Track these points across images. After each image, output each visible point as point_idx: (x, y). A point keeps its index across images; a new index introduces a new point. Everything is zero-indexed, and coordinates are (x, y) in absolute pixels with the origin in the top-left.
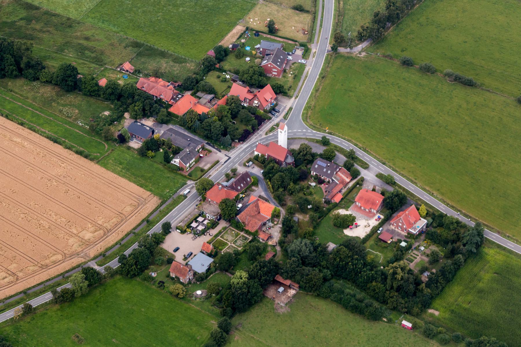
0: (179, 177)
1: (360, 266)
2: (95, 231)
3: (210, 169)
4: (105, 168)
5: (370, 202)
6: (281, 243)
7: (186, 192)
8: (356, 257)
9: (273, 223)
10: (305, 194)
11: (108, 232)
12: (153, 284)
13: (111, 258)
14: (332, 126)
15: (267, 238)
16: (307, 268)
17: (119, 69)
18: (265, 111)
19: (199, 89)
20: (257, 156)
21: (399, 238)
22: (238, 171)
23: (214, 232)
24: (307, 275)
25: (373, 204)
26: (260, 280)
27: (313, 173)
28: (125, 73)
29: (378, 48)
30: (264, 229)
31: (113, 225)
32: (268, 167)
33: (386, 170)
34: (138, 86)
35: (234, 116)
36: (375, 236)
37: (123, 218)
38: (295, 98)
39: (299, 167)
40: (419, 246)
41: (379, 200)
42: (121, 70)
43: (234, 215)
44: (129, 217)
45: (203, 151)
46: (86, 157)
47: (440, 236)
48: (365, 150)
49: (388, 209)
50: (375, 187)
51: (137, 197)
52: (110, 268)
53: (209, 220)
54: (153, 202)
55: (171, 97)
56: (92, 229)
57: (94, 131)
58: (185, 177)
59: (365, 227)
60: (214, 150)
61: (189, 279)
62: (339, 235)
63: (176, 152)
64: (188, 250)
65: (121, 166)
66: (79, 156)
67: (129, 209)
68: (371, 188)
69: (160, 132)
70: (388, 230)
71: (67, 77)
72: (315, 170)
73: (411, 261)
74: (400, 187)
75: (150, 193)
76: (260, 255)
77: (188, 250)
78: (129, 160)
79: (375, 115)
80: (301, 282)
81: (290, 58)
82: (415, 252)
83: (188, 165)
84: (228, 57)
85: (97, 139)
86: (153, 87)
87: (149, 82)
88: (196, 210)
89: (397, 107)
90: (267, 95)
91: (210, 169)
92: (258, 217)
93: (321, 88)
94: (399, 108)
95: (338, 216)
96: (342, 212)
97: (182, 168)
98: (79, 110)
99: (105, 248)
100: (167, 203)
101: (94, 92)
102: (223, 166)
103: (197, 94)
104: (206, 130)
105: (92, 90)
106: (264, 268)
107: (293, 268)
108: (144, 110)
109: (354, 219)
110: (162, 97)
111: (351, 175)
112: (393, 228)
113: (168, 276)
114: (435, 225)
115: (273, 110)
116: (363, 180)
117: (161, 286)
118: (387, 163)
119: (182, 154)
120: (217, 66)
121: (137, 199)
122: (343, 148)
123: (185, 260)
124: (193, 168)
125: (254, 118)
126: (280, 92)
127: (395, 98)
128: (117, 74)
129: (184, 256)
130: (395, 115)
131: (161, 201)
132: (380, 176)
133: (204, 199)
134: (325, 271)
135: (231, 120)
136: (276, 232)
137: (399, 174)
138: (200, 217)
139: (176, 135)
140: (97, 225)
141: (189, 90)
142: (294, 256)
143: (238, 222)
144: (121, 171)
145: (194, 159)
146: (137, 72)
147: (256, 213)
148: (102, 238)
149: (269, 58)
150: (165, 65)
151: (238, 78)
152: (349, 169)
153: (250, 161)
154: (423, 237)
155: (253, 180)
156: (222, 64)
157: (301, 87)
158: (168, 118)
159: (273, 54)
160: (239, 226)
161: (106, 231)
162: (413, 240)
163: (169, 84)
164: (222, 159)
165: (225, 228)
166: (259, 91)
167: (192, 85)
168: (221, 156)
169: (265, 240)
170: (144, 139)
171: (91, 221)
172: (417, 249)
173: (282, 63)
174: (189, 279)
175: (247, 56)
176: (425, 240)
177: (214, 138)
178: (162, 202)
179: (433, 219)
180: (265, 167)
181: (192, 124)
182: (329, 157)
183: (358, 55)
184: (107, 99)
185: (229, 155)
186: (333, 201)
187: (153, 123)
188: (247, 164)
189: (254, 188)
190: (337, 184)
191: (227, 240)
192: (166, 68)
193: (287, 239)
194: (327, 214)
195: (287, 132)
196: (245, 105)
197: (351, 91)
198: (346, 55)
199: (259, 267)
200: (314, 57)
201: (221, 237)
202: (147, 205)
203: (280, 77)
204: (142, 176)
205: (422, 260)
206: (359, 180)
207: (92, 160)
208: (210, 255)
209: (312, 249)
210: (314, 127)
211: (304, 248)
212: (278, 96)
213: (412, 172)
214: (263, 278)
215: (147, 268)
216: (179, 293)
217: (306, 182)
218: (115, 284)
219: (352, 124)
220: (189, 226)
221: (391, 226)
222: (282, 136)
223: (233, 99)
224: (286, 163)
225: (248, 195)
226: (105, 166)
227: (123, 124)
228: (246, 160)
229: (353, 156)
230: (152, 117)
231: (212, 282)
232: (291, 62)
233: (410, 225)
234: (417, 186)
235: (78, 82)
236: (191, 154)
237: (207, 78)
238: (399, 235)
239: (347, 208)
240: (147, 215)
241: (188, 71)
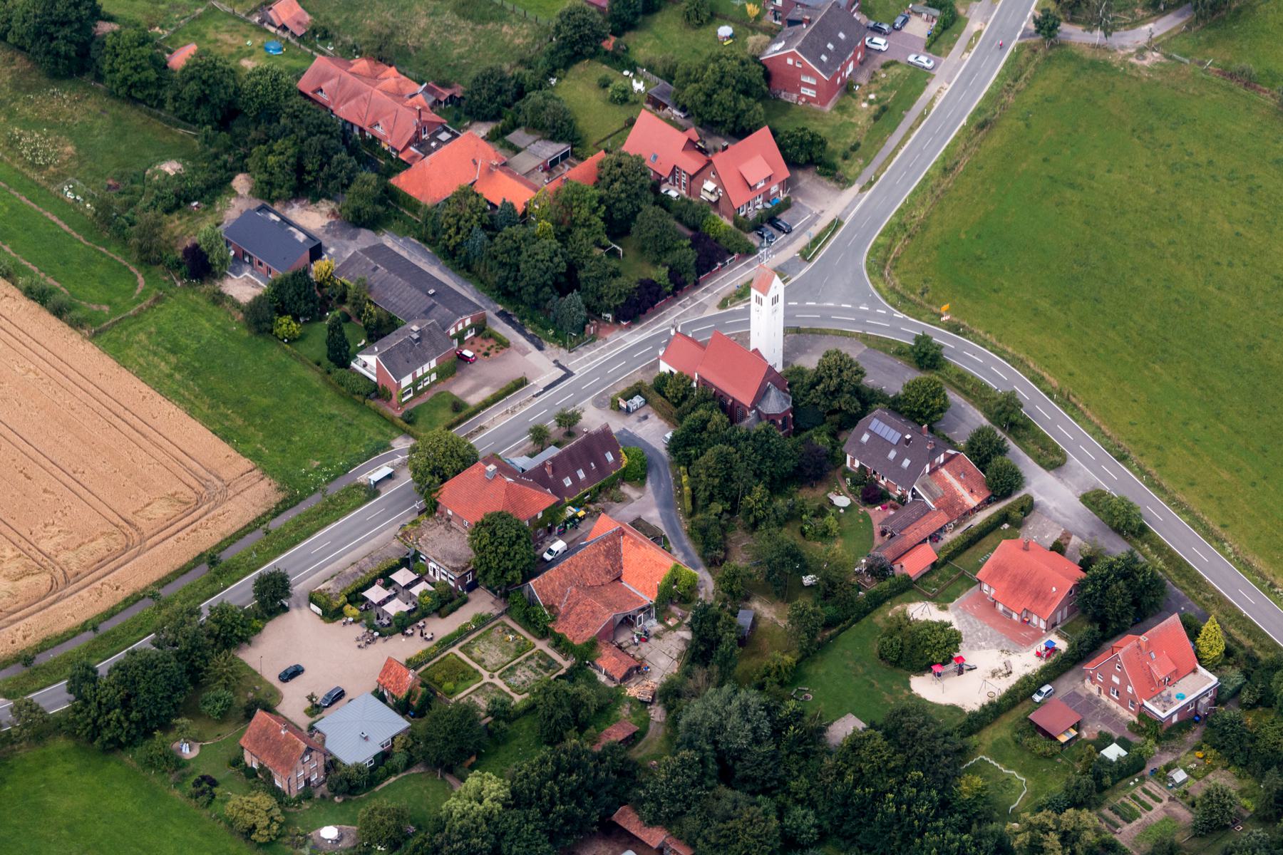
0: (367, 419)
1: (923, 810)
2: (24, 574)
3: (486, 404)
4: (117, 359)
5: (1025, 587)
6: (670, 694)
7: (376, 476)
8: (916, 774)
9: (661, 621)
10: (803, 534)
11: (67, 582)
12: (177, 785)
13: (50, 674)
14: (968, 303)
15: (623, 670)
16: (730, 793)
17: (257, 19)
18: (739, 224)
19: (521, 118)
20: (663, 380)
21: (1106, 729)
22: (582, 422)
23: (440, 628)
24: (726, 818)
25: (1040, 595)
26: (545, 813)
27: (853, 463)
28: (275, 35)
29: (1210, 42)
30: (625, 638)
31: (90, 560)
32: (686, 422)
33: (1120, 481)
34: (305, 84)
35: (618, 227)
36: (1019, 711)
37: (132, 540)
38: (862, 190)
39: (804, 435)
40: (1168, 768)
41: (1062, 579)
42: (262, 22)
43: (518, 573)
44: (156, 539)
45: (478, 341)
46: (59, 312)
47: (1253, 740)
48: (1065, 402)
49: (1091, 622)
50: (1067, 535)
51: (202, 472)
52: (33, 708)
53: (433, 584)
54: (253, 495)
55: (411, 134)
56: (14, 566)
57: (108, 223)
58: (390, 422)
59: (994, 674)
60: (522, 340)
61: (308, 782)
62: (891, 692)
63: (378, 330)
64: (332, 680)
65: (173, 359)
66: (35, 306)
67: (160, 511)
68: (1051, 536)
69: (345, 255)
70: (1073, 697)
71: (54, 23)
72: (861, 450)
73: (1129, 817)
74: (1160, 548)
75: (250, 466)
76: (582, 728)
77: (332, 680)
78: (209, 342)
79: (1138, 282)
80: (699, 841)
81: (880, 42)
82: (1152, 786)
83: (407, 381)
84: (659, 18)
85: (113, 253)
86: (355, 94)
87: (345, 75)
88: (395, 544)
89: (1224, 261)
90: (755, 164)
91: (486, 404)
92: (609, 593)
93: (965, 161)
94: (1230, 265)
95: (903, 623)
96: (922, 612)
97: (385, 389)
98: (79, 147)
99: (43, 635)
100: (303, 507)
101: (146, 87)
102: (537, 401)
103: (510, 138)
104: (502, 265)
105: (136, 78)
106: (570, 773)
107: (677, 787)
108: (299, 169)
109: (954, 640)
110: (380, 131)
111: (989, 485)
112: (1094, 689)
113: (237, 762)
114: (1245, 697)
115: (771, 221)
116: (1028, 507)
117: (203, 792)
118: (1133, 455)
119: (393, 340)
120: (609, 44)
121: (198, 478)
122: (987, 386)
123: (312, 715)
124: (427, 396)
125: (688, 242)
126: (810, 163)
127: (1227, 226)
128: (246, 37)
129: (310, 698)
130: (1211, 288)
131: (282, 495)
132: (1093, 500)
133: (432, 508)
134: (799, 811)
135: (605, 240)
136: (664, 655)
137: (1168, 503)
138: (404, 571)
139: (390, 271)
140: (34, 552)
141: (485, 119)
142: (690, 745)
143: (532, 602)
144: (171, 376)
145: (433, 363)
146: (319, 34)
147: (607, 579)
148: (38, 602)
149: (795, 36)
150: (423, 22)
151: (667, 93)
152: (982, 463)
153: (639, 393)
154: (1193, 737)
155: (625, 461)
156: (630, 38)
157: (894, 153)
158: (386, 208)
159: (809, 22)
160: (535, 620)
161: (61, 580)
162: (1151, 742)
163: (420, 89)
164: (539, 373)
165: (482, 621)
166: (725, 148)
167: (497, 103)
168: (540, 363)
169: (618, 678)
170: (278, 274)
171: (15, 538)
172: (1163, 776)
173: (839, 57)
174: (308, 782)
175: (726, 20)
176: (1199, 748)
177: (525, 297)
178: (284, 501)
179: (1247, 676)
180: (681, 418)
181: (458, 239)
182: (922, 412)
183: (1133, 60)
184: (184, 118)
185: (570, 365)
186: (897, 567)
187: (326, 221)
188: (623, 404)
189: (626, 489)
190: (929, 510)
191: (480, 662)
192: (426, 32)
193: (691, 684)
194: (867, 613)
195: (781, 304)
196: (673, 194)
197: (1072, 186)
198: (1088, 54)
199: (550, 768)
200: (968, 49)
201: (461, 649)
202: (230, 506)
203: (828, 108)
204: (240, 403)
205: (1171, 817)
206: (1011, 507)
207: (77, 324)
208: (402, 708)
209: (766, 728)
210: (902, 300)
211: (735, 719)
212: (800, 174)
213: (1219, 499)
214: (560, 808)
215: (166, 727)
216: (254, 827)
217: (820, 491)
218: (44, 767)
219: (1044, 304)
220: (355, 597)
221: (1088, 682)
222: (761, 318)
223: (620, 165)
224: (759, 414)
225: (593, 515)
226: (118, 353)
227: (221, 212)
228: (623, 387)
229: (1013, 418)
230: (329, 198)
231: (386, 803)
232: (883, 59)
233: (1154, 687)
234: (1222, 549)
235: (93, 46)
236: (425, 342)
237: (565, 82)
238: (1109, 716)
239: (942, 599)
240: (219, 539)
241: (500, 51)
